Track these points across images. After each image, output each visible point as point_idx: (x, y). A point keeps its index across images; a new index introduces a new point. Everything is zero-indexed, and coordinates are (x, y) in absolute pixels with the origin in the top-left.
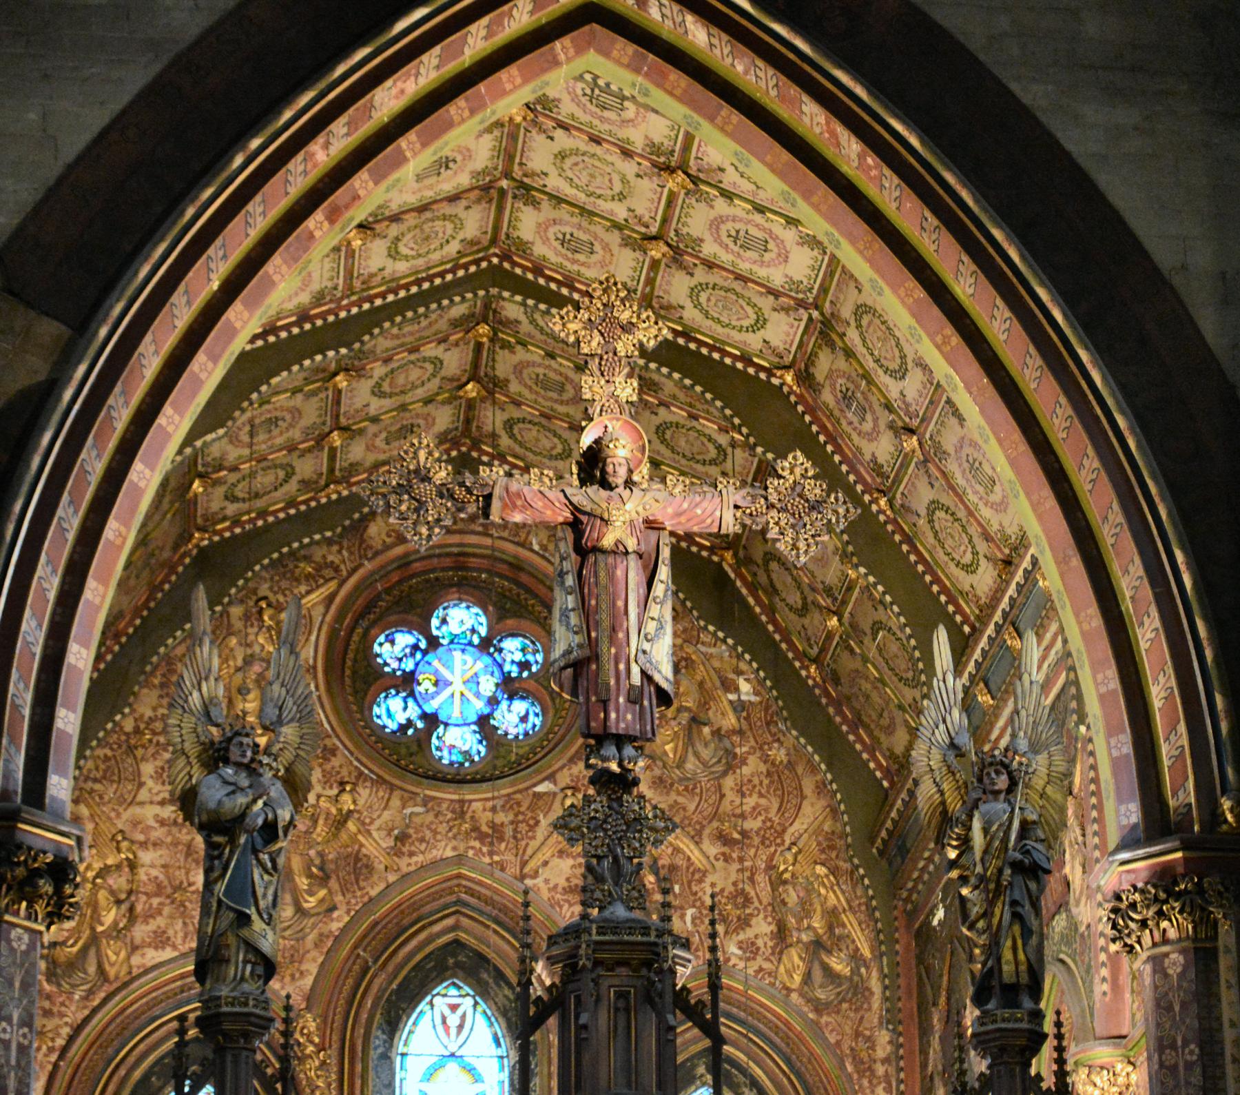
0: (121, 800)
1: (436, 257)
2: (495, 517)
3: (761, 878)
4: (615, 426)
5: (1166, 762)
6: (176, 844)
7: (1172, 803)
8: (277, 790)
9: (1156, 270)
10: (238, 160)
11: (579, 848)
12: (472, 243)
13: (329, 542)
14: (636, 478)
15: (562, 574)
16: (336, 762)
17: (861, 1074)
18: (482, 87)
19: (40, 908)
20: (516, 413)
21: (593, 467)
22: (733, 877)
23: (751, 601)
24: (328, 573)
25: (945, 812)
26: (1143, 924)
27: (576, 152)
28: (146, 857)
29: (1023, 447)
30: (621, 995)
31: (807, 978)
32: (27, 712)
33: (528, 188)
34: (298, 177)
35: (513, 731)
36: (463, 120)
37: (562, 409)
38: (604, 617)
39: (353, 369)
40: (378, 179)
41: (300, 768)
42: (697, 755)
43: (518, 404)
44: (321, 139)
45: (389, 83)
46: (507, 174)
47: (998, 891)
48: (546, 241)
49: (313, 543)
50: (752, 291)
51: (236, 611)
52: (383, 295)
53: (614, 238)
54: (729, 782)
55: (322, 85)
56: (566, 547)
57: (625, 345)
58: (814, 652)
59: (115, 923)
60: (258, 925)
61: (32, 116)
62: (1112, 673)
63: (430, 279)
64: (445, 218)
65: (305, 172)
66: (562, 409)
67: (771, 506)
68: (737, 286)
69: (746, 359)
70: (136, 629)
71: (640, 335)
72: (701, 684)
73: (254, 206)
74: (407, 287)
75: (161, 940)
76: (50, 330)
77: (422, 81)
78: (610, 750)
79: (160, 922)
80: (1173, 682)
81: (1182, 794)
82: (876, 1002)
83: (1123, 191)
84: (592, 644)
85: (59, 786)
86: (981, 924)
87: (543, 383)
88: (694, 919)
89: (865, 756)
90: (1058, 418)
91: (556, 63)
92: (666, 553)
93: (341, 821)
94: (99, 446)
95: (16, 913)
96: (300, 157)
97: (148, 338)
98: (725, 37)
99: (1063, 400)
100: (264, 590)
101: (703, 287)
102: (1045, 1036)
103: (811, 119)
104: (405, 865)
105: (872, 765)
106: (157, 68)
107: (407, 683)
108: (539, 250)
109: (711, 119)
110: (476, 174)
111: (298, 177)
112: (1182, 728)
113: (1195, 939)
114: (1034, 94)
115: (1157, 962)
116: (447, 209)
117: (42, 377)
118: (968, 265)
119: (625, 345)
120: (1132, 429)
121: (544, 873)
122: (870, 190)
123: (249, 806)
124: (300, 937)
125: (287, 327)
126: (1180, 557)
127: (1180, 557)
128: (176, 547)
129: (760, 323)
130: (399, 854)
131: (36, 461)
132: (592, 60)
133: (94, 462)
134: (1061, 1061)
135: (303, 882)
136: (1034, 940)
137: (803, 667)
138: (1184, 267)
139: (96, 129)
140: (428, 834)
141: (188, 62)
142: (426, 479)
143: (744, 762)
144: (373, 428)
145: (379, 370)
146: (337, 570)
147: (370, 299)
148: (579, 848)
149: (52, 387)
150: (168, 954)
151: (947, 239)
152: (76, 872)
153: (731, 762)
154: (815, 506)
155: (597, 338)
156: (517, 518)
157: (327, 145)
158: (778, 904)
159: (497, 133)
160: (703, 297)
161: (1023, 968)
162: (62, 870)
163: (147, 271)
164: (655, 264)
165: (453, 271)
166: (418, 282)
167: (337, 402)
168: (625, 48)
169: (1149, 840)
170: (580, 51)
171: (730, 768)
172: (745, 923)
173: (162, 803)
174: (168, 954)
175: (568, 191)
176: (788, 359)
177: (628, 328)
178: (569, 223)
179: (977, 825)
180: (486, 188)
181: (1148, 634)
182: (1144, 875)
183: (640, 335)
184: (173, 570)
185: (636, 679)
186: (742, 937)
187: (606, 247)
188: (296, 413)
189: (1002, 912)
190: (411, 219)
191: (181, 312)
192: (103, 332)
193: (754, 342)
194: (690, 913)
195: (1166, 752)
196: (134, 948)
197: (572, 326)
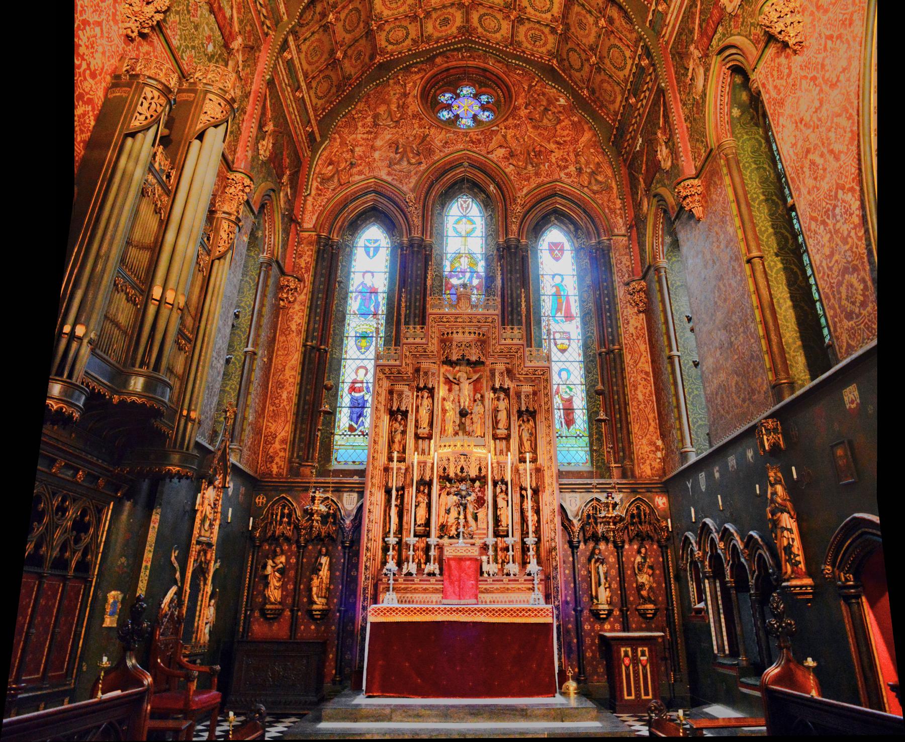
0: (350, 133)
3: (571, 154)
17: (611, 213)
31: (590, 183)
54: (558, 127)
79: (361, 167)
82: (615, 191)
104: (446, 150)
107: (449, 107)
130: (444, 147)
143: (563, 121)
158: (577, 162)
194: (547, 164)
196: (351, 175)
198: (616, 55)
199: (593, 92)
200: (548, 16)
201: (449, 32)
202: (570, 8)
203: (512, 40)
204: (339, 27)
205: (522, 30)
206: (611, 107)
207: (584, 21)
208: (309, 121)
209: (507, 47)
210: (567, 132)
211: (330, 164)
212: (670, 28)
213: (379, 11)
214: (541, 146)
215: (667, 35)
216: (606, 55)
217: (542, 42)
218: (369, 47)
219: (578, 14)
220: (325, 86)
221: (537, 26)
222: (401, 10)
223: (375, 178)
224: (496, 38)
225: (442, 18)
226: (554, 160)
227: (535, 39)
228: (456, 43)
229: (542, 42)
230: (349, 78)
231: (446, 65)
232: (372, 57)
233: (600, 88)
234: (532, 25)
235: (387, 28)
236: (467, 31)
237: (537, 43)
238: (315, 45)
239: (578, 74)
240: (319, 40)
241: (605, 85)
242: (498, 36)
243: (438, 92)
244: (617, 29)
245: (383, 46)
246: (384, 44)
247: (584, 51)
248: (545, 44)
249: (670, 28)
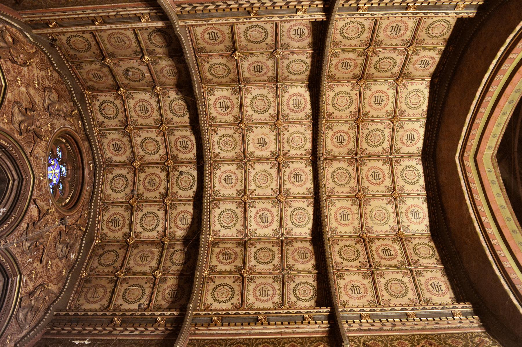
23: (91, 251)
54: (57, 260)
70: (71, 74)
88: (29, 262)
89: (71, 298)
105: (70, 301)
137: (83, 271)
140: (38, 166)
198: (137, 293)
199: (88, 280)
200: (139, 229)
201: (108, 152)
202: (152, 245)
203: (106, 205)
204: (134, 64)
205: (121, 210)
206: (82, 301)
207: (149, 259)
208: (61, 26)
209: (101, 199)
210: (55, 269)
211: (13, 40)
212: (208, 332)
213: (134, 96)
214: (44, 250)
215: (201, 332)
216: (130, 284)
217: (113, 228)
218: (101, 86)
219: (152, 253)
220: (81, 45)
221: (128, 222)
222: (133, 114)
223: (6, 86)
224: (106, 190)
225: (122, 146)
226: (35, 265)
227: (115, 221)
228: (98, 157)
229: (113, 228)
230: (79, 67)
231: (84, 151)
232: (91, 88)
233: (97, 286)
234: (127, 217)
235: (118, 102)
236: (108, 166)
237: (110, 224)
238: (127, 42)
239: (96, 264)
240: (129, 47)
241: (101, 290)
242: (109, 191)
243: (63, 146)
244: (160, 287)
245: (99, 98)
246: (102, 99)
247: (123, 264)
248: (112, 231)
249: (208, 332)
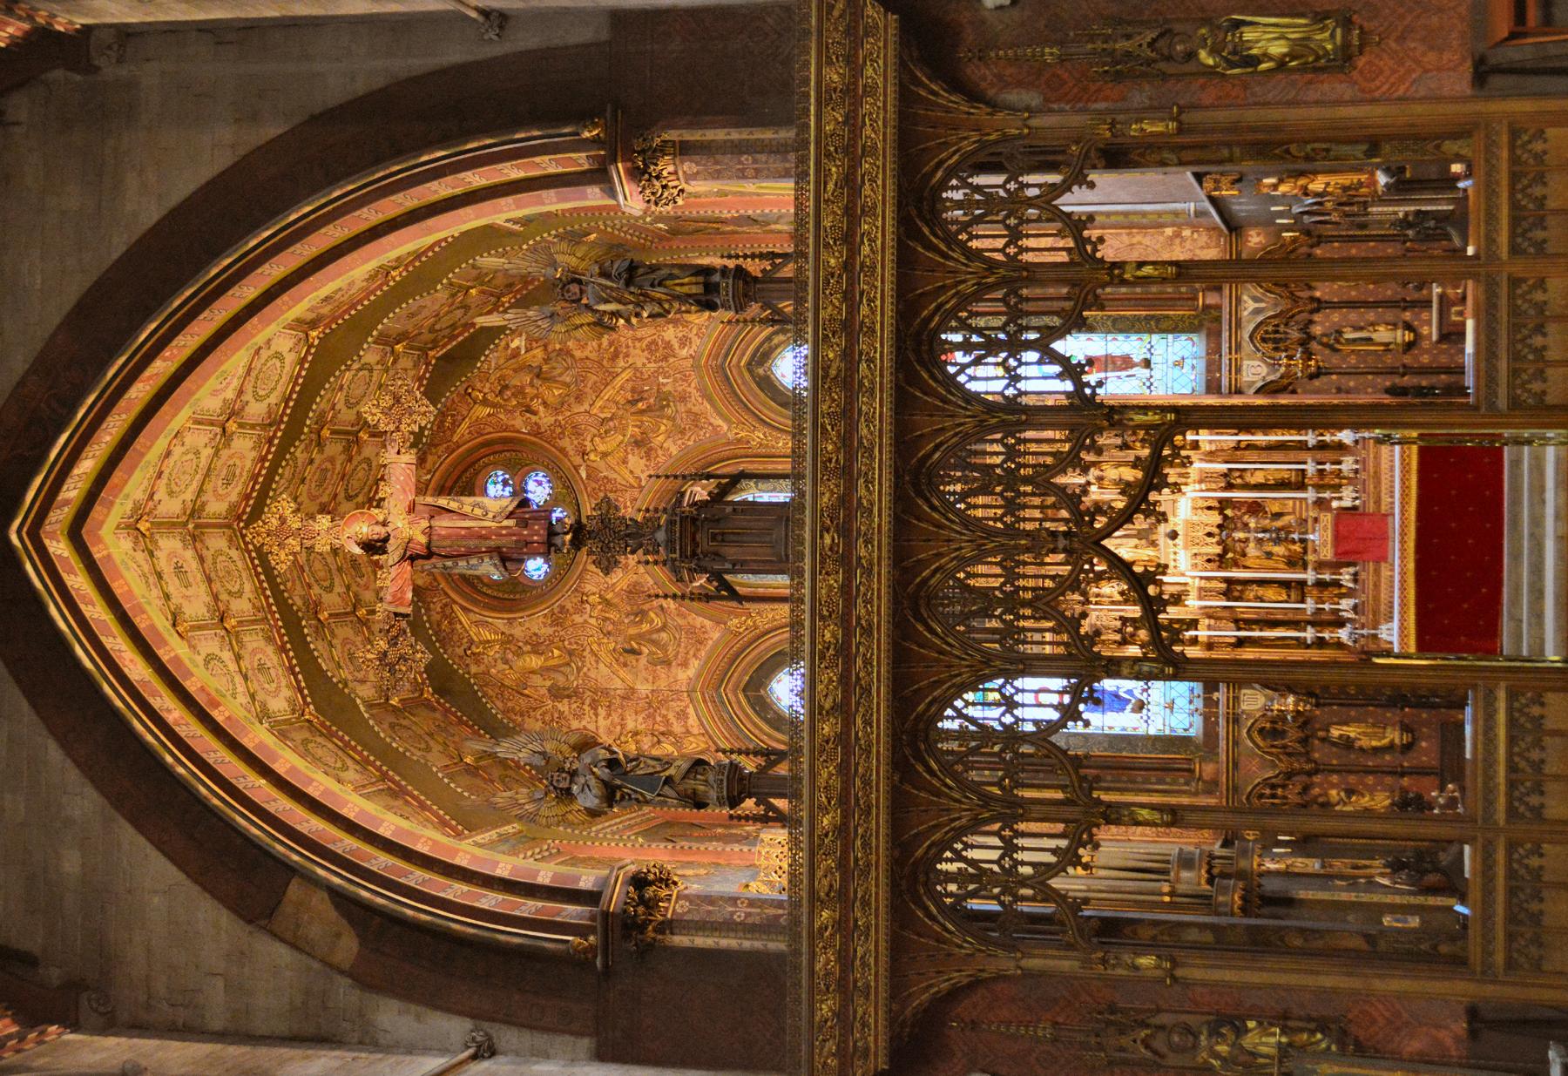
1: (240, 564)
2: (409, 610)
4: (350, 531)
5: (560, 170)
6: (622, 707)
7: (586, 167)
8: (587, 759)
9: (235, 165)
10: (181, 770)
11: (622, 559)
12: (230, 540)
13: (428, 610)
14: (381, 518)
15: (445, 567)
16: (569, 606)
18: (126, 606)
19: (663, 893)
20: (342, 495)
21: (374, 547)
22: (638, 351)
24: (448, 611)
25: (595, 324)
26: (664, 187)
27: (168, 485)
28: (630, 725)
29: (355, 255)
30: (714, 537)
32: (540, 904)
33: (193, 511)
34: (190, 729)
35: (548, 490)
36: (149, 618)
37: (338, 467)
38: (472, 543)
39: (315, 608)
40: (190, 674)
41: (573, 739)
42: (561, 375)
43: (336, 495)
44: (164, 715)
45: (126, 670)
46: (185, 525)
47: (646, 295)
48: (228, 494)
49: (429, 621)
50: (257, 364)
51: (474, 669)
52: (267, 598)
53: (225, 453)
54: (578, 354)
55: (129, 715)
56: (428, 564)
57: (294, 523)
58: (493, 299)
59: (672, 744)
60: (672, 771)
61: (156, 900)
62: (502, 201)
63: (255, 567)
64: (215, 563)
65: (187, 724)
66: (338, 467)
67: (398, 429)
68: (253, 374)
69: (302, 361)
71: (288, 512)
72: (515, 371)
73: (210, 759)
74: (261, 582)
75: (682, 715)
76: (295, 890)
77: (124, 647)
78: (558, 540)
79: (671, 716)
80: (508, 164)
81: (581, 161)
83: (184, 185)
84: (490, 551)
85: (587, 881)
86: (667, 306)
87: (321, 483)
90: (335, 233)
91: (109, 556)
92: (429, 500)
93: (608, 603)
94: (369, 858)
95: (667, 909)
96: (177, 729)
97: (298, 827)
98: (88, 448)
99: (323, 230)
100: (460, 651)
101: (255, 394)
102: (738, 268)
103: (141, 392)
106: (122, 821)
108: (234, 497)
109: (142, 455)
110: (185, 547)
111: (190, 729)
112: (537, 159)
113: (674, 155)
114: (119, 244)
115: (689, 178)
116: (209, 561)
117: (326, 895)
118: (235, 290)
119: (294, 523)
120: (341, 187)
121: (638, 472)
122: (187, 352)
123: (597, 778)
124: (679, 628)
125: (290, 660)
126: (425, 158)
127: (425, 158)
128: (434, 709)
129: (279, 356)
131: (380, 901)
132: (107, 532)
133: (380, 861)
134: (753, 256)
135: (645, 627)
136: (676, 271)
138: (233, 146)
139: (163, 859)
141: (117, 800)
142: (385, 654)
144: (354, 588)
145: (316, 590)
146: (446, 605)
147: (269, 605)
148: (622, 559)
149: (336, 894)
150: (691, 710)
151: (217, 304)
152: (640, 872)
153: (565, 352)
154: (397, 400)
155: (290, 540)
156: (410, 595)
157: (169, 711)
159: (157, 537)
160: (261, 393)
161: (693, 279)
162: (639, 881)
163: (255, 830)
164: (241, 426)
165: (249, 552)
166: (258, 574)
167: (337, 615)
168: (98, 510)
169: (610, 181)
170: (99, 540)
171: (569, 353)
172: (668, 345)
173: (596, 715)
174: (691, 710)
175: (195, 485)
176: (302, 335)
177: (283, 520)
178: (216, 482)
179: (602, 307)
180: (194, 538)
181: (476, 179)
182: (634, 186)
183: (288, 512)
184: (447, 711)
185: (511, 522)
186: (676, 346)
187: (230, 457)
188: (345, 641)
189: (658, 293)
190: (216, 586)
191: (281, 805)
192: (295, 858)
193: (290, 358)
195: (553, 169)
196: (688, 732)
197: (283, 557)
